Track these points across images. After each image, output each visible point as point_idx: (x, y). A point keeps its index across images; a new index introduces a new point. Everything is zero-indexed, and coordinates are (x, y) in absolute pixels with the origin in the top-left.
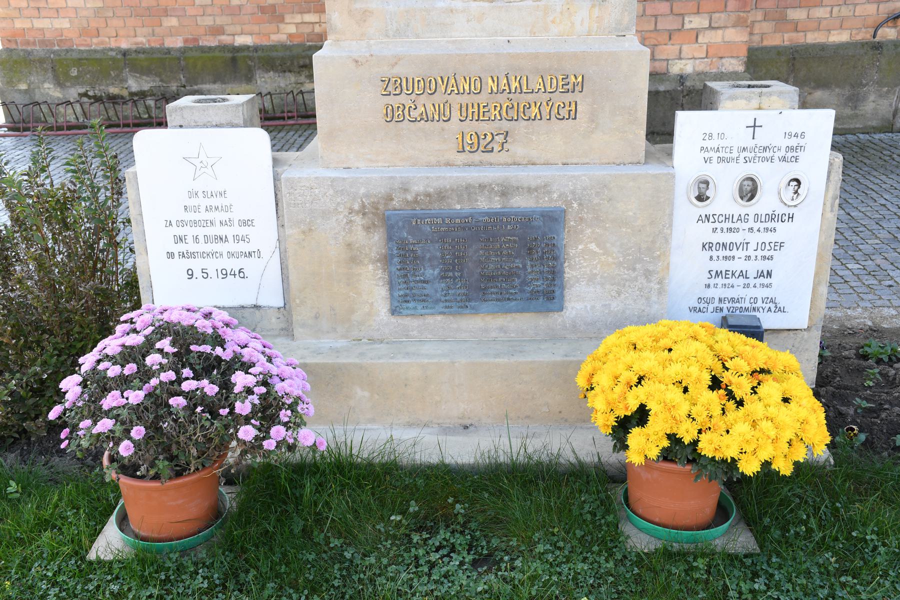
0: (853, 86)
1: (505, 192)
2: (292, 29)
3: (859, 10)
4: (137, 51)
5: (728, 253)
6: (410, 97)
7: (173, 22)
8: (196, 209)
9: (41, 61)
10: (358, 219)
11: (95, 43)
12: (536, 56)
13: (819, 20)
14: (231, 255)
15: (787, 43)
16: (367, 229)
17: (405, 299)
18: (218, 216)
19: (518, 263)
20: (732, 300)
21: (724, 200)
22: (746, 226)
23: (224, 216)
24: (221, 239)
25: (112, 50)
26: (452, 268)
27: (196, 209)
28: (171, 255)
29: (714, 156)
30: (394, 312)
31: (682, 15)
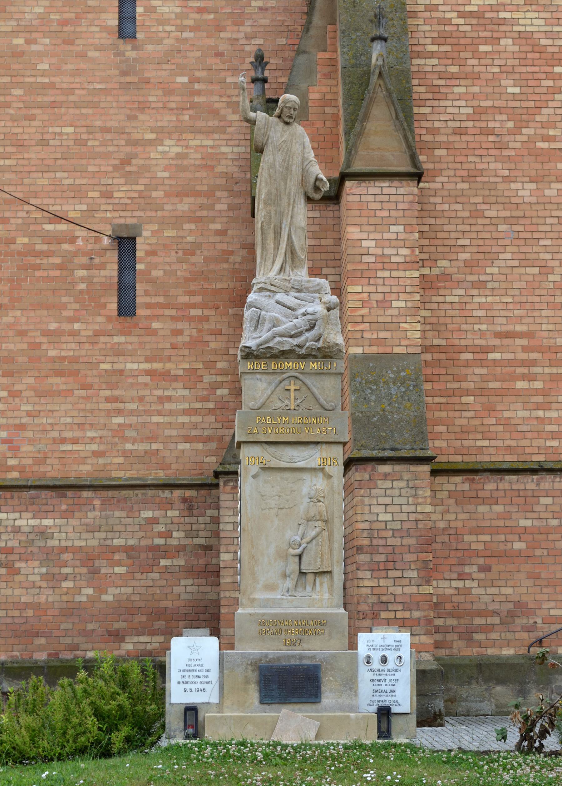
0: (520, 684)
1: (301, 657)
2: (130, 647)
3: (518, 636)
5: (379, 683)
6: (270, 626)
7: (43, 641)
8: (190, 665)
10: (249, 667)
14: (201, 683)
16: (253, 671)
17: (265, 697)
20: (382, 701)
21: (376, 664)
22: (385, 673)
24: (198, 677)
27: (190, 665)
28: (179, 683)
29: (372, 648)
30: (261, 702)
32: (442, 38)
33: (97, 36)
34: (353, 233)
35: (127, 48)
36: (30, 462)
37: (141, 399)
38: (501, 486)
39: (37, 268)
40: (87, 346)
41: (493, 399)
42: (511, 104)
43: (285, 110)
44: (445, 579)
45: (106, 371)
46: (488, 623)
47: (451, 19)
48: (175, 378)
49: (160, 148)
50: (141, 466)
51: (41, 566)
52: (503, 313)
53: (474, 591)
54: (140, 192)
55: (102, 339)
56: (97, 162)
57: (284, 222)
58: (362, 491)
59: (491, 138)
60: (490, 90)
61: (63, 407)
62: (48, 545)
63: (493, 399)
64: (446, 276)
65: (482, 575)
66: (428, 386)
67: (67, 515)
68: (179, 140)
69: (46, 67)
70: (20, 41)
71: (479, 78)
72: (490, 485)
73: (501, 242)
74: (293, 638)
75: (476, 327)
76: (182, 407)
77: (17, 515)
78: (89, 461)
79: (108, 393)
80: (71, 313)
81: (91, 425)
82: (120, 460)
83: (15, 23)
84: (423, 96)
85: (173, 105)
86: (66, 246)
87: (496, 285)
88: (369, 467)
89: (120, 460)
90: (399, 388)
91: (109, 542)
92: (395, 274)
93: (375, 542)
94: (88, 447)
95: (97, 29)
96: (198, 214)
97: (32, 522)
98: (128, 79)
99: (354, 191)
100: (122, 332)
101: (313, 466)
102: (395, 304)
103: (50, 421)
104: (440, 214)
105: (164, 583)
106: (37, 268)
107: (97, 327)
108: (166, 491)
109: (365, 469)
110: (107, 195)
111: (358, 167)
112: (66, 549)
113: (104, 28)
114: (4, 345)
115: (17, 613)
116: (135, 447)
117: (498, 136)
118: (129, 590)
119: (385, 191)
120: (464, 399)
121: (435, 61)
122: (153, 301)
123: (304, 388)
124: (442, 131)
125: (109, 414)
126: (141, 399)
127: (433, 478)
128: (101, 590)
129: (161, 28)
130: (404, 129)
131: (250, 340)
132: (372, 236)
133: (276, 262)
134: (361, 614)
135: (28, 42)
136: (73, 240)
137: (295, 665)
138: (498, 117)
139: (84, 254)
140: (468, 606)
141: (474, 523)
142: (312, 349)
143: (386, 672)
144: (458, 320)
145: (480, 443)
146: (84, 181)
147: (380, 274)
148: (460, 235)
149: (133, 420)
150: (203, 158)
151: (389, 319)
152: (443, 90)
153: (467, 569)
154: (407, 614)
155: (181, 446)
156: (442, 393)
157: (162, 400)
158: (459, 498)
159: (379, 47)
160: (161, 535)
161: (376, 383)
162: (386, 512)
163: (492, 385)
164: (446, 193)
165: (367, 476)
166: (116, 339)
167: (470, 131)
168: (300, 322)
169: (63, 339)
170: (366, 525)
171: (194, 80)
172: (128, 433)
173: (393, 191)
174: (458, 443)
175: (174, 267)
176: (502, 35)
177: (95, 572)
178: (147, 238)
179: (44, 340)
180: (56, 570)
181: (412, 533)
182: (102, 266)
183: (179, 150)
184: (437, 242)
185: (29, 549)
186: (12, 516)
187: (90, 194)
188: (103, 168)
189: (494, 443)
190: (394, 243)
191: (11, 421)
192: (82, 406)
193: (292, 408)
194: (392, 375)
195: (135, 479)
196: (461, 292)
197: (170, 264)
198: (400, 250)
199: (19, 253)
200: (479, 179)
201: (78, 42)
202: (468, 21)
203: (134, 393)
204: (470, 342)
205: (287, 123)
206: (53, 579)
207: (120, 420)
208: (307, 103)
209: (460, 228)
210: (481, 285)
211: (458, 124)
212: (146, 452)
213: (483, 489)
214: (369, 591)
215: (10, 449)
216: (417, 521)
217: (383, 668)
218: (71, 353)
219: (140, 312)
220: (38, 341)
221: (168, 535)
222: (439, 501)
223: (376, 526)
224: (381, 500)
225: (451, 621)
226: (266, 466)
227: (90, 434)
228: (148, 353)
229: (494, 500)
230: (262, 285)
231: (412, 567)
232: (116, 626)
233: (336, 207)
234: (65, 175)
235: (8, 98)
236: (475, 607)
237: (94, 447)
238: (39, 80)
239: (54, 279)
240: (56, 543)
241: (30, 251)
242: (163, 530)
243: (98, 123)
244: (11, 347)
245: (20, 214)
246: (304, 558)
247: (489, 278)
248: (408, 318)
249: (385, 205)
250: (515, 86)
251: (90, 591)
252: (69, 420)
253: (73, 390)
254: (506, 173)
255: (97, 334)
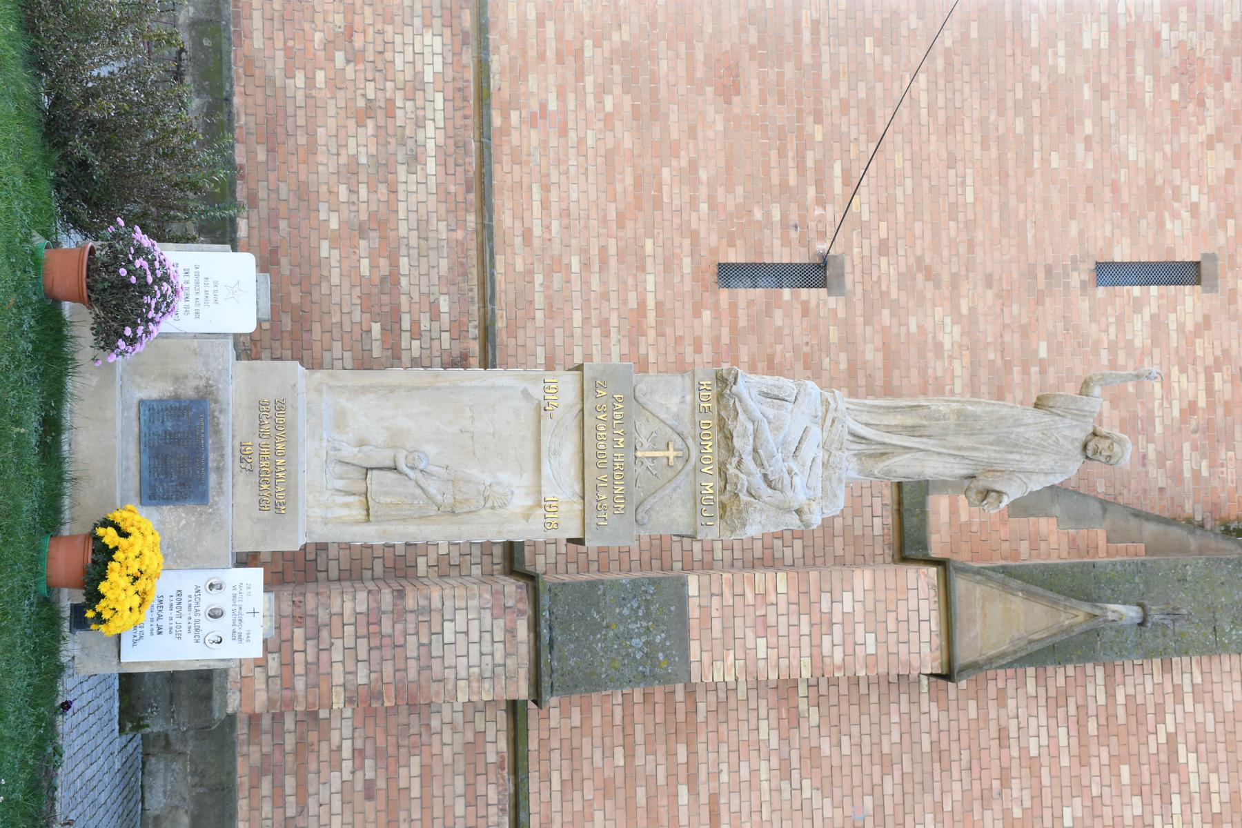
1: (219, 470)
4: (230, 113)
6: (274, 415)
7: (262, 157)
8: (206, 285)
9: (218, 11)
10: (203, 383)
11: (238, 70)
12: (296, 486)
13: (259, 809)
15: (239, 780)
16: (197, 388)
18: (202, 296)
19: (175, 477)
21: (210, 600)
22: (192, 616)
23: (202, 301)
25: (232, 87)
26: (173, 438)
27: (206, 285)
29: (237, 592)
30: (141, 402)
31: (280, 651)
32: (1135, 709)
33: (1099, 233)
34: (863, 578)
35: (1084, 273)
36: (515, 142)
37: (605, 296)
38: (493, 810)
39: (782, 153)
40: (677, 221)
41: (621, 794)
42: (1047, 814)
43: (1108, 442)
44: (354, 729)
45: (643, 247)
46: (288, 799)
47: (1165, 723)
48: (634, 344)
49: (948, 320)
50: (511, 297)
51: (368, 156)
52: (745, 806)
53: (335, 775)
54: (887, 293)
55: (687, 242)
56: (928, 234)
57: (932, 442)
58: (487, 596)
59: (996, 784)
60: (1066, 782)
61: (592, 189)
62: (399, 167)
63: (621, 794)
64: (795, 719)
65: (359, 786)
66: (638, 696)
67: (443, 193)
68: (960, 346)
69: (1054, 164)
70: (1089, 128)
71: (1081, 766)
72: (494, 793)
73: (847, 800)
74: (255, 458)
75: (724, 767)
76: (595, 352)
77: (441, 124)
78: (518, 224)
79: (612, 250)
80: (720, 200)
81: (568, 227)
82: (520, 267)
83: (1113, 121)
84: (1050, 682)
85: (1007, 338)
86: (812, 192)
87: (786, 795)
88: (526, 606)
89: (520, 267)
90: (641, 650)
91: (404, 251)
92: (805, 641)
93: (411, 617)
94: (537, 223)
95: (1108, 234)
96: (861, 374)
97: (431, 145)
98: (1041, 275)
99: (923, 579)
100: (696, 269)
101: (544, 489)
102: (762, 642)
103: (572, 170)
104: (884, 710)
105: (347, 328)
106: (782, 153)
107: (703, 234)
108: (477, 331)
109: (521, 600)
110: (883, 248)
111: (961, 585)
112: (393, 191)
113: (1110, 243)
114: (675, 107)
115: (301, 121)
116: (537, 288)
117: (1000, 794)
118: (335, 280)
119: (924, 625)
120: (619, 752)
121: (1102, 700)
122: (740, 312)
123: (670, 473)
124: (1002, 711)
125: (584, 251)
126: (605, 296)
127: (504, 706)
128: (335, 241)
129: (1112, 320)
130: (1015, 652)
131: (749, 386)
132: (858, 606)
133: (868, 429)
134: (301, 598)
135: (1088, 140)
136: (821, 202)
137: (206, 460)
138: (1026, 794)
139: (802, 218)
140: (313, 766)
141: (437, 771)
142: (736, 484)
143: (194, 618)
144: (733, 740)
145: (555, 776)
146: (901, 217)
147: (805, 619)
148: (855, 740)
149: (576, 285)
150: (936, 378)
151: (739, 634)
152: (1061, 711)
153: (369, 763)
154: (299, 669)
155: (540, 351)
156: (628, 716)
157: (604, 323)
158: (474, 749)
159: (1133, 614)
160: (415, 323)
161: (647, 615)
162: (456, 633)
163: (641, 792)
164: (915, 717)
165: (510, 603)
166: (687, 261)
167: (1005, 752)
168: (777, 468)
169: (685, 189)
170: (436, 603)
171: (1043, 366)
172: (557, 278)
173: (925, 637)
174: (555, 744)
175: (787, 340)
176: (1147, 801)
177: (362, 231)
178: (825, 303)
179: (684, 163)
180: (363, 177)
181: (425, 674)
182: (786, 242)
183: (947, 346)
184: (844, 705)
185: (392, 140)
186: (439, 116)
187: (883, 225)
188: (918, 242)
189: (557, 797)
190: (849, 639)
191: (571, 116)
192: (593, 214)
193: (639, 454)
194: (658, 639)
195: (493, 288)
196: (774, 744)
197: (792, 335)
198: (841, 648)
199: (801, 129)
200: (937, 765)
201: (1090, 206)
202: (1164, 748)
203: (613, 286)
204: (702, 757)
205: (1085, 447)
206: (351, 171)
207: (576, 267)
208: (1033, 515)
209: (866, 739)
210: (785, 772)
211: (1013, 734)
212: (531, 302)
213: (487, 784)
214: (336, 609)
215: (533, 114)
216: (443, 680)
217: (202, 612)
218: (666, 199)
219: (724, 294)
220: (682, 153)
221: (416, 334)
222: (470, 718)
223: (436, 618)
224: (474, 626)
225: (290, 741)
226: (543, 412)
227: (555, 226)
228: (668, 305)
229: (473, 799)
230: (833, 405)
231: (373, 676)
232: (284, 261)
233: (889, 559)
234: (909, 191)
235: (1010, 113)
236: (312, 777)
237: (537, 231)
238: (1037, 155)
239: (767, 173)
240: (402, 176)
241: (804, 143)
242: (423, 328)
243: (980, 236)
244: (673, 117)
245: (854, 130)
246: (391, 475)
247: (796, 785)
248: (742, 662)
249: (903, 626)
250: (1074, 819)
251: (334, 225)
252: (574, 196)
253: (615, 201)
254: (948, 808)
255: (694, 236)
